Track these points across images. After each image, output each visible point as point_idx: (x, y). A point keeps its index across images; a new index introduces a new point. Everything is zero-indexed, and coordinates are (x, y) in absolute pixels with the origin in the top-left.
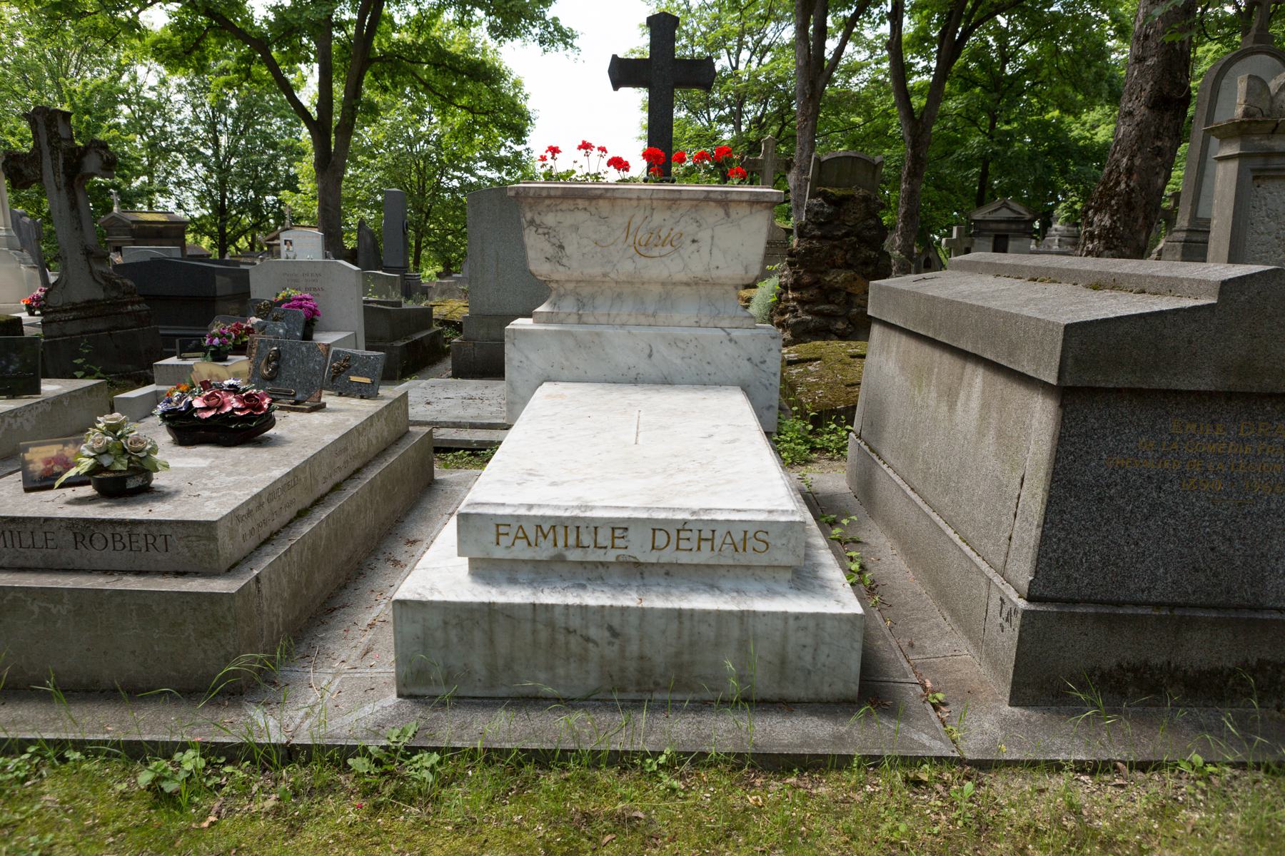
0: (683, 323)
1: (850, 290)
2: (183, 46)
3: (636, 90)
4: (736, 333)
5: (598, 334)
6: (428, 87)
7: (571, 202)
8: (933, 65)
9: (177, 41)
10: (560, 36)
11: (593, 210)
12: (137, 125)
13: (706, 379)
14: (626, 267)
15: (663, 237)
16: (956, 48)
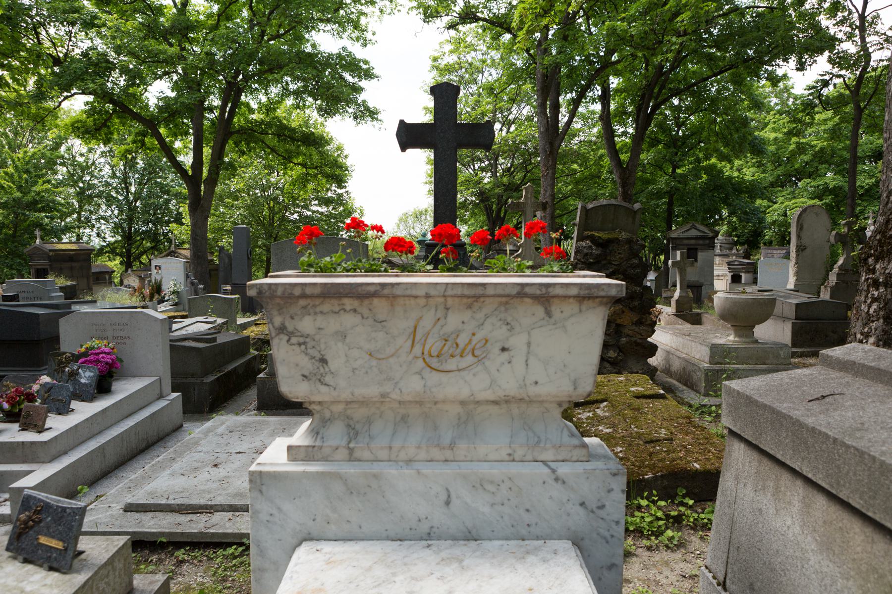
0: (491, 457)
1: (619, 321)
2: (95, 125)
3: (423, 150)
4: (564, 470)
5: (376, 476)
6: (273, 150)
7: (335, 302)
8: (631, 130)
9: (90, 122)
10: (368, 113)
11: (365, 312)
12: (72, 180)
13: (524, 532)
14: (413, 385)
15: (461, 346)
16: (649, 118)
